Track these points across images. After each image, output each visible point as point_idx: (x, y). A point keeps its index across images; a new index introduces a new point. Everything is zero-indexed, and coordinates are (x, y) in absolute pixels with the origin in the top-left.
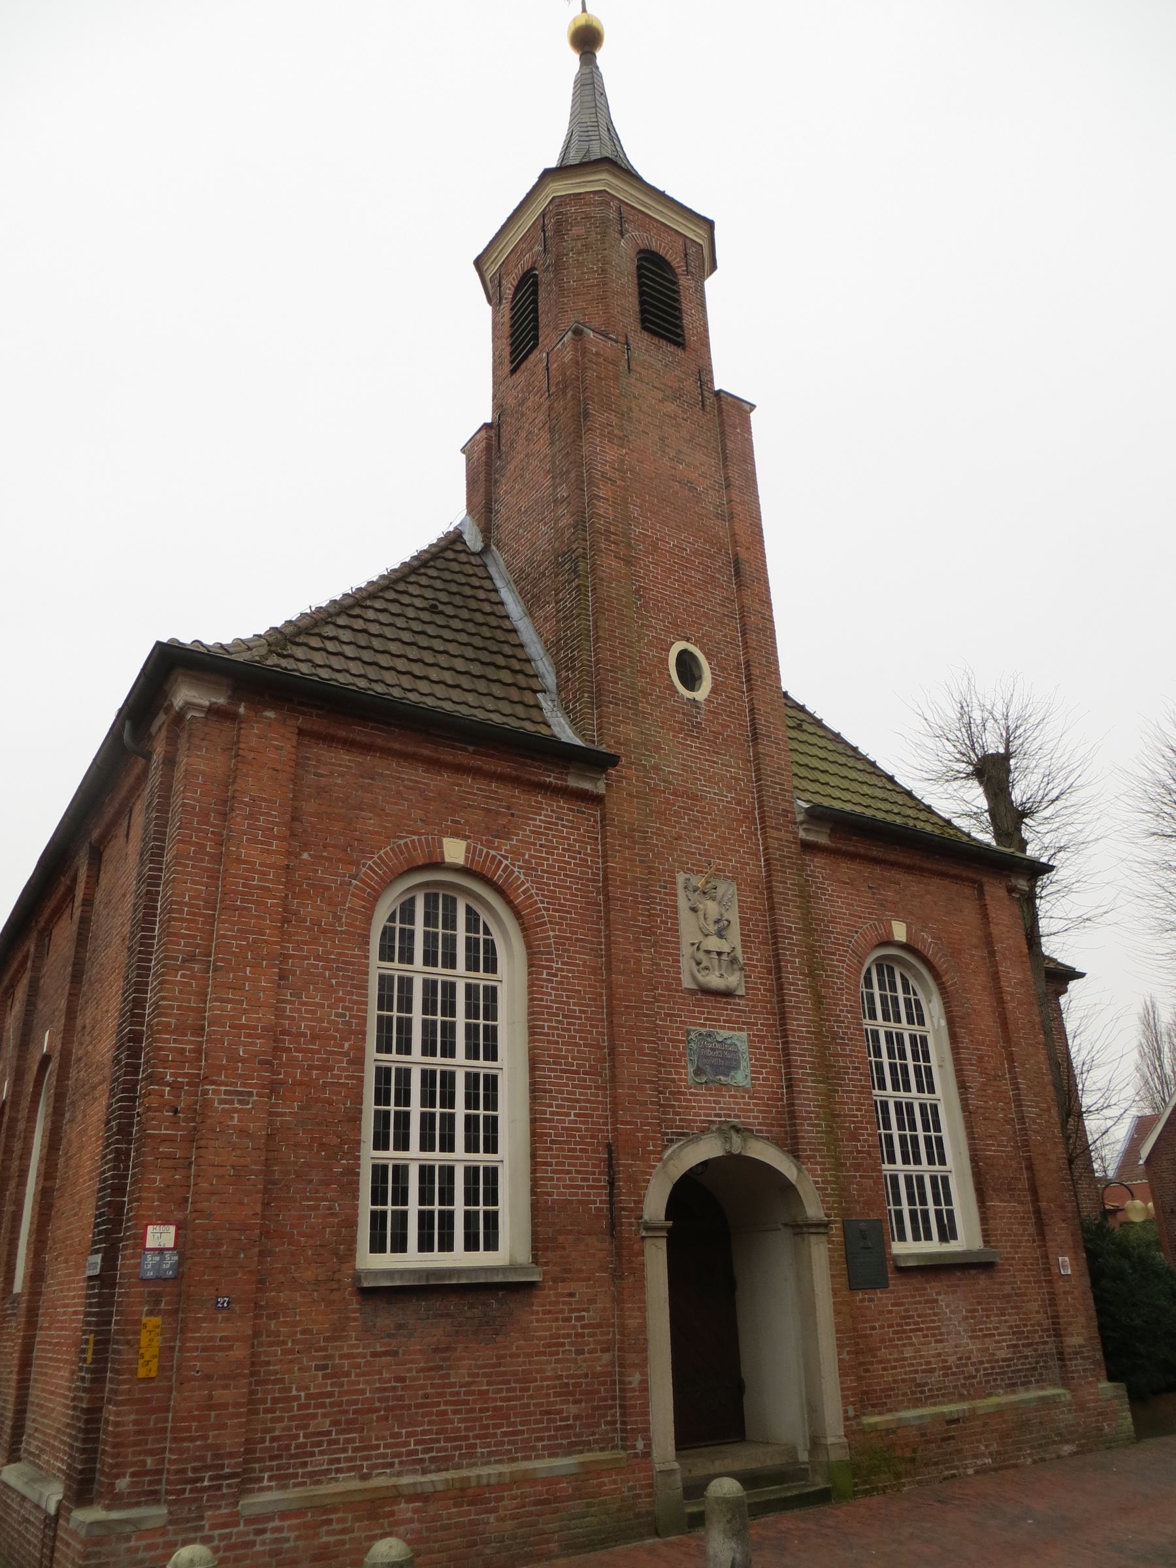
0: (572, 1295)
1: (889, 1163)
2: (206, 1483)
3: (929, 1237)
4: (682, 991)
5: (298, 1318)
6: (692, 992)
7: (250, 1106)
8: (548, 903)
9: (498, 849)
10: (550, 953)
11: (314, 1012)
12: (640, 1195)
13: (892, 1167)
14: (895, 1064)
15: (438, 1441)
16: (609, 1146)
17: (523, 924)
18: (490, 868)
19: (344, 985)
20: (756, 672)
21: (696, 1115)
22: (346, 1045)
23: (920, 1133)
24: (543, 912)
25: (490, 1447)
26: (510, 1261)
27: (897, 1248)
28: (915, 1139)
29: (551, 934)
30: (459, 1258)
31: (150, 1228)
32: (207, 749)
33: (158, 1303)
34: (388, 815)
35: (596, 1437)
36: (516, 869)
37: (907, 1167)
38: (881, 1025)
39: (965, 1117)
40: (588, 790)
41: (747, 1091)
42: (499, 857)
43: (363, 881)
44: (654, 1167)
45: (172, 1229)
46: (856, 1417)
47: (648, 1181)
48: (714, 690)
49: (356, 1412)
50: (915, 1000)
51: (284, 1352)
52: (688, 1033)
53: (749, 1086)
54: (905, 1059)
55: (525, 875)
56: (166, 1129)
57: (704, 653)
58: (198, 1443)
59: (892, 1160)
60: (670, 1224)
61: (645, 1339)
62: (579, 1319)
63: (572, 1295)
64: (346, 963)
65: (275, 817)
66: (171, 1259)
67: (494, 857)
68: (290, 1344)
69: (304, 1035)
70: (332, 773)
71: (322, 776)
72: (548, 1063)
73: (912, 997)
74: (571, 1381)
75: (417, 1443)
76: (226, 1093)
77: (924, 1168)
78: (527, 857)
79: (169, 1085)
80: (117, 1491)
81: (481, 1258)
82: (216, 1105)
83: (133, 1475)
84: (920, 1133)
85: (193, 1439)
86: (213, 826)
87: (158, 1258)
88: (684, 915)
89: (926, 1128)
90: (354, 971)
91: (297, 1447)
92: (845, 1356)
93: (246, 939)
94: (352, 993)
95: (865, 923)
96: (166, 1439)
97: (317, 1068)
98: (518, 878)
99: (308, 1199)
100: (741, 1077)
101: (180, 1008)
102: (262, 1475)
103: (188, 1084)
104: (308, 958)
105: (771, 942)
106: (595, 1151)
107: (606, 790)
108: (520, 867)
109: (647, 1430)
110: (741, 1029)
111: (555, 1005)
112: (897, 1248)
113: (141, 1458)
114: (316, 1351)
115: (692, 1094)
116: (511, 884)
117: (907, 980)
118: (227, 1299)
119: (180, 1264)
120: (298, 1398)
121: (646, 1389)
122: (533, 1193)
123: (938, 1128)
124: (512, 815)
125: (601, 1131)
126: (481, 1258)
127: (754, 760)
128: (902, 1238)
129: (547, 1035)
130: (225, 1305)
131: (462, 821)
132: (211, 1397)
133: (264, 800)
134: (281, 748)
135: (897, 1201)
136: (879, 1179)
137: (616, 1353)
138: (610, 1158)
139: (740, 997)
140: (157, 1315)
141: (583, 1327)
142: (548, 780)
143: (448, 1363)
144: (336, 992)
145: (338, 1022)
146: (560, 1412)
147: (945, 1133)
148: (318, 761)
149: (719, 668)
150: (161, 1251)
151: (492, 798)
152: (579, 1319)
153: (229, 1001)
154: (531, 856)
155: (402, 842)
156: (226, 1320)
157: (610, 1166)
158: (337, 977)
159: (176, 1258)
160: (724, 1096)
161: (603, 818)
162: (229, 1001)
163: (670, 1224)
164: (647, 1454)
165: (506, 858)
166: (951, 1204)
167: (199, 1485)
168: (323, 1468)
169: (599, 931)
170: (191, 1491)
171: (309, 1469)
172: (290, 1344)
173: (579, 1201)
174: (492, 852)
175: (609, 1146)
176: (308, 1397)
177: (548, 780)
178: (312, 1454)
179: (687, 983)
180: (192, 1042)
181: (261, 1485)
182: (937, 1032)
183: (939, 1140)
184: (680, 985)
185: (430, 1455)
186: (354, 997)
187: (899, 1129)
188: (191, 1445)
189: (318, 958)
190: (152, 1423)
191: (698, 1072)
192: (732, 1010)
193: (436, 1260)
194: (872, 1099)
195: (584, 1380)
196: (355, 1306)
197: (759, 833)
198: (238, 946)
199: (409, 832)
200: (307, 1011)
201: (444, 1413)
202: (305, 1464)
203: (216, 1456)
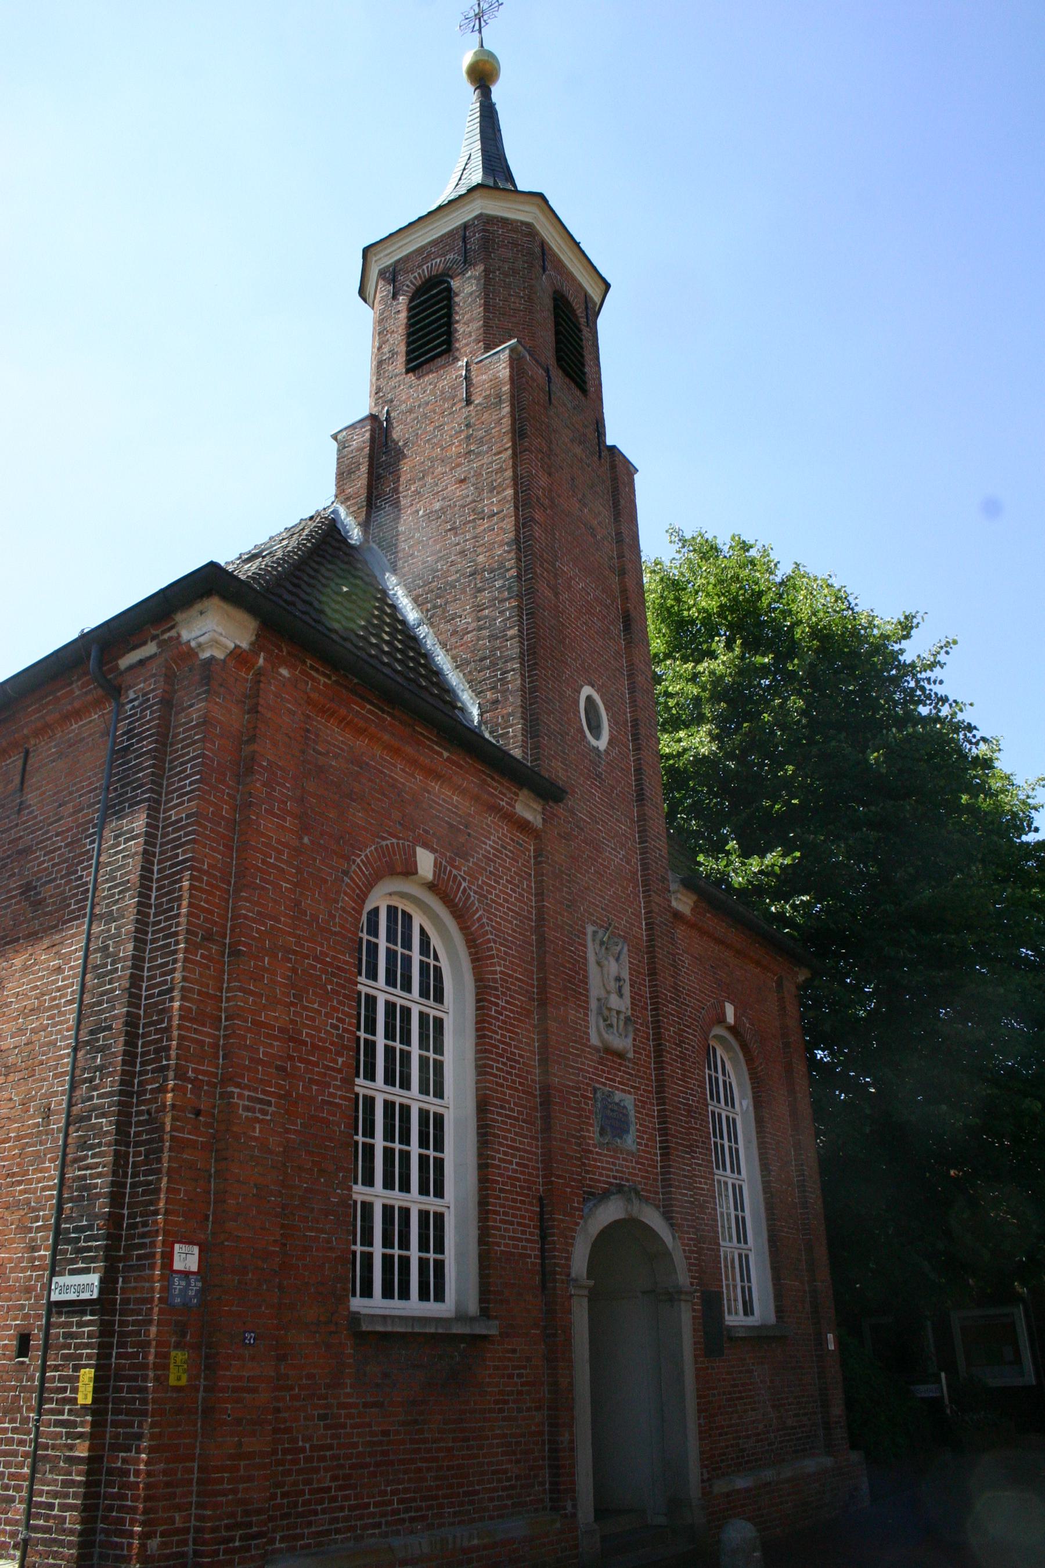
0: (514, 1351)
1: (363, 1184)
2: (237, 1544)
3: (405, 1295)
4: (589, 1047)
5: (303, 1361)
6: (597, 1049)
7: (268, 1118)
8: (496, 935)
9: (458, 868)
10: (496, 989)
11: (313, 1019)
12: (567, 1252)
13: (367, 1190)
14: (394, 1049)
15: (414, 1500)
16: (541, 1199)
17: (476, 953)
18: (452, 888)
19: (337, 993)
20: (643, 731)
21: (601, 1175)
22: (340, 1060)
23: (415, 1149)
24: (492, 944)
25: (115, 1555)
26: (456, 1312)
27: (357, 1303)
28: (405, 1156)
29: (498, 968)
30: (414, 1306)
31: (177, 1246)
32: (224, 698)
33: (184, 1335)
34: (373, 810)
35: (532, 1498)
36: (472, 894)
37: (388, 1193)
38: (381, 991)
39: (765, 1199)
40: (529, 822)
41: (633, 1154)
42: (459, 878)
43: (352, 879)
44: (577, 1224)
45: (196, 1249)
46: (709, 1479)
47: (573, 1238)
48: (610, 742)
49: (352, 1467)
50: (435, 966)
51: (293, 1398)
52: (595, 1090)
53: (635, 1151)
54: (409, 1044)
55: (479, 902)
56: (189, 1133)
57: (604, 703)
58: (230, 1497)
59: (369, 1181)
60: (592, 1283)
61: (573, 1399)
62: (520, 1376)
63: (514, 1351)
64: (339, 968)
65: (287, 788)
66: (196, 1285)
67: (455, 877)
68: (297, 1390)
69: (305, 1043)
70: (328, 753)
71: (320, 753)
72: (496, 1106)
73: (432, 962)
74: (514, 1440)
75: (401, 1501)
76: (250, 1098)
77: (415, 1201)
78: (480, 882)
79: (191, 1081)
80: (149, 1553)
81: (431, 1308)
82: (240, 1112)
83: (163, 1534)
84: (415, 1149)
85: (224, 1493)
86: (228, 787)
87: (184, 1283)
88: (593, 969)
89: (423, 1143)
90: (345, 979)
91: (303, 1505)
92: (702, 1421)
93: (265, 924)
94: (344, 1004)
95: (709, 1001)
96: (191, 1493)
97: (317, 1083)
98: (473, 903)
99: (311, 1230)
100: (630, 1141)
101: (200, 993)
102: (275, 1535)
103: (209, 1083)
104: (307, 957)
105: (649, 1008)
106: (531, 1204)
107: (543, 825)
108: (475, 892)
109: (574, 1491)
110: (630, 1093)
111: (501, 1046)
112: (357, 1303)
113: (170, 1514)
114: (319, 1399)
115: (598, 1153)
116: (468, 909)
117: (428, 937)
118: (253, 1335)
119: (202, 1292)
120: (303, 1449)
121: (572, 1449)
122: (481, 1241)
123: (439, 1146)
124: (469, 835)
125: (535, 1183)
126: (431, 1308)
127: (638, 821)
128: (367, 1292)
129: (495, 1076)
130: (252, 1341)
131: (431, 832)
132: (240, 1444)
133: (280, 768)
134: (294, 713)
135: (368, 1240)
136: (345, 1201)
137: (546, 1412)
138: (542, 1213)
139: (630, 1060)
140: (183, 1349)
141: (523, 1384)
142: (501, 803)
143: (422, 1418)
144: (331, 1000)
145: (333, 1034)
146: (505, 1472)
147: (449, 1155)
148: (317, 736)
149: (614, 721)
150: (186, 1274)
151: (453, 813)
152: (520, 1376)
153: (251, 993)
154: (483, 882)
155: (384, 843)
156: (253, 1358)
157: (542, 1220)
158: (331, 983)
159: (199, 1284)
160: (618, 1158)
161: (538, 853)
162: (251, 993)
163: (592, 1283)
164: (574, 1515)
165: (464, 879)
166: (442, 1252)
167: (231, 1545)
168: (325, 1528)
169: (532, 972)
170: (226, 1552)
171: (313, 1529)
172: (297, 1390)
173: (520, 1254)
174: (455, 872)
175: (541, 1199)
176: (313, 1448)
177: (501, 803)
178: (315, 1513)
179: (595, 1041)
180: (209, 1035)
181: (274, 1547)
182: (744, 1113)
183: (440, 1164)
184: (588, 1040)
185: (410, 1514)
186: (346, 1009)
187: (421, 1146)
188: (224, 1499)
189: (316, 958)
190: (179, 1474)
191: (602, 1132)
192: (624, 1072)
193: (396, 1306)
194: (352, 1091)
195: (522, 1440)
196: (350, 1351)
197: (641, 895)
198: (258, 931)
199: (390, 834)
200: (308, 1017)
201: (419, 1470)
202: (310, 1524)
203: (246, 1513)
